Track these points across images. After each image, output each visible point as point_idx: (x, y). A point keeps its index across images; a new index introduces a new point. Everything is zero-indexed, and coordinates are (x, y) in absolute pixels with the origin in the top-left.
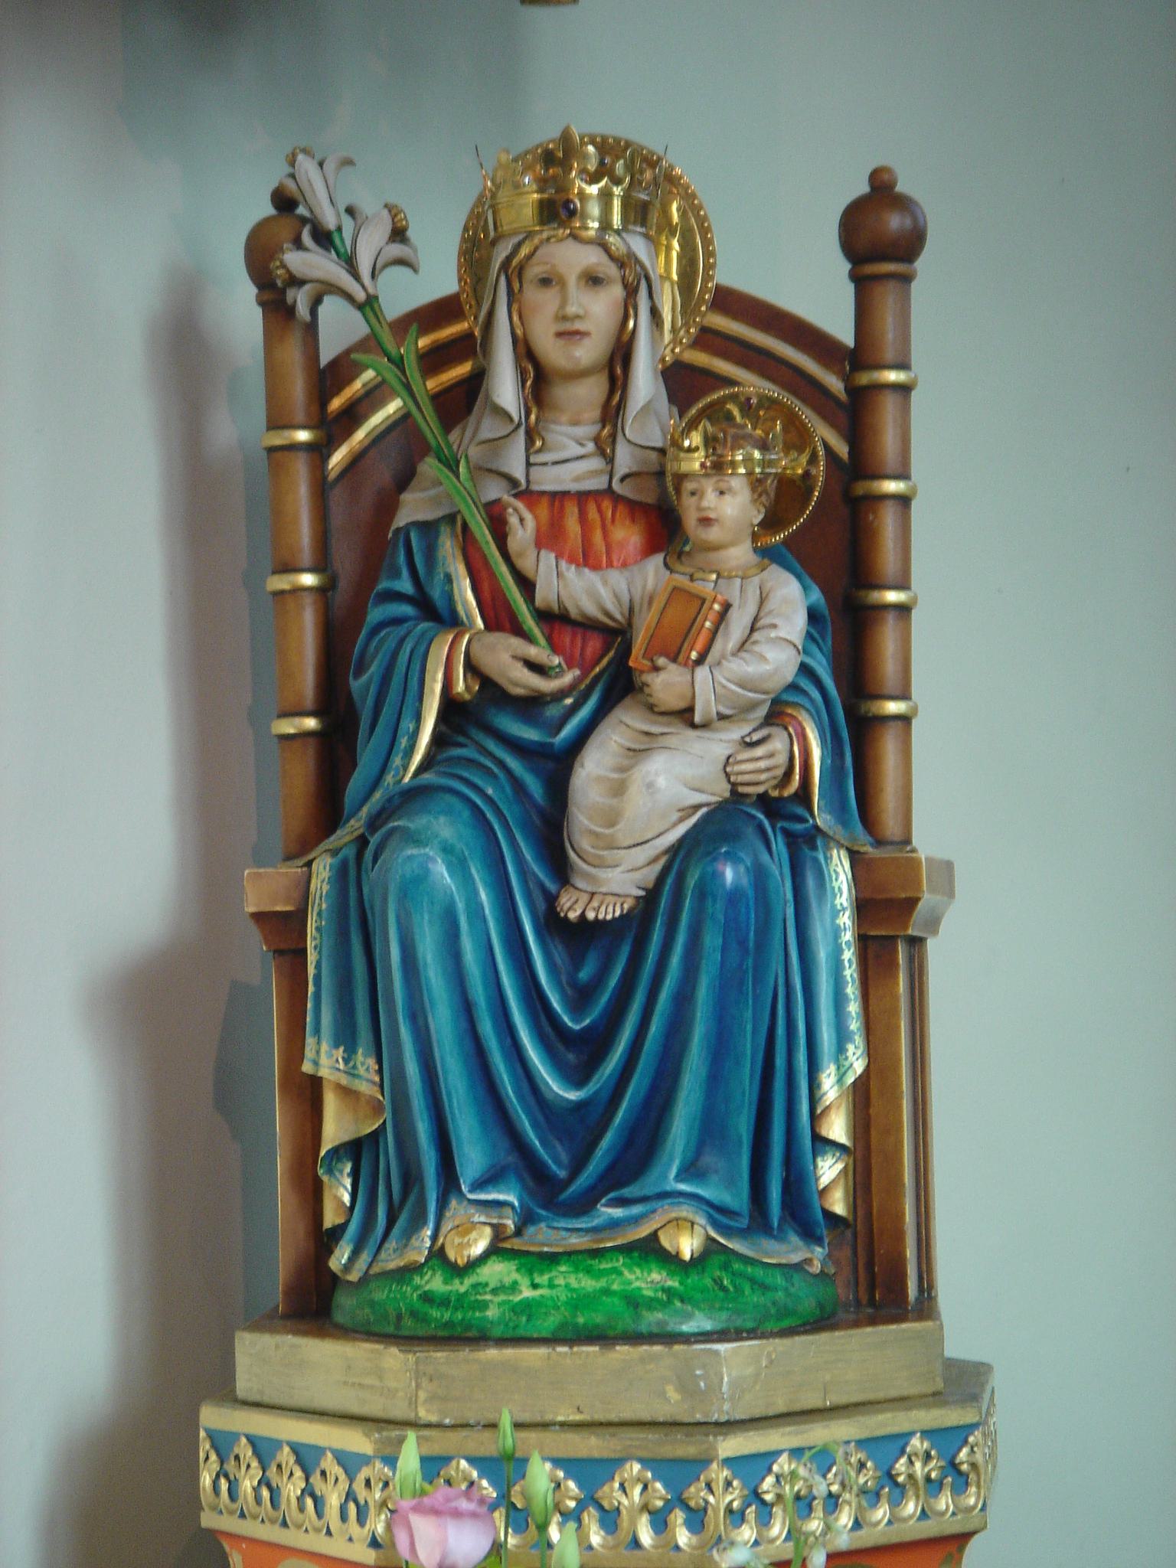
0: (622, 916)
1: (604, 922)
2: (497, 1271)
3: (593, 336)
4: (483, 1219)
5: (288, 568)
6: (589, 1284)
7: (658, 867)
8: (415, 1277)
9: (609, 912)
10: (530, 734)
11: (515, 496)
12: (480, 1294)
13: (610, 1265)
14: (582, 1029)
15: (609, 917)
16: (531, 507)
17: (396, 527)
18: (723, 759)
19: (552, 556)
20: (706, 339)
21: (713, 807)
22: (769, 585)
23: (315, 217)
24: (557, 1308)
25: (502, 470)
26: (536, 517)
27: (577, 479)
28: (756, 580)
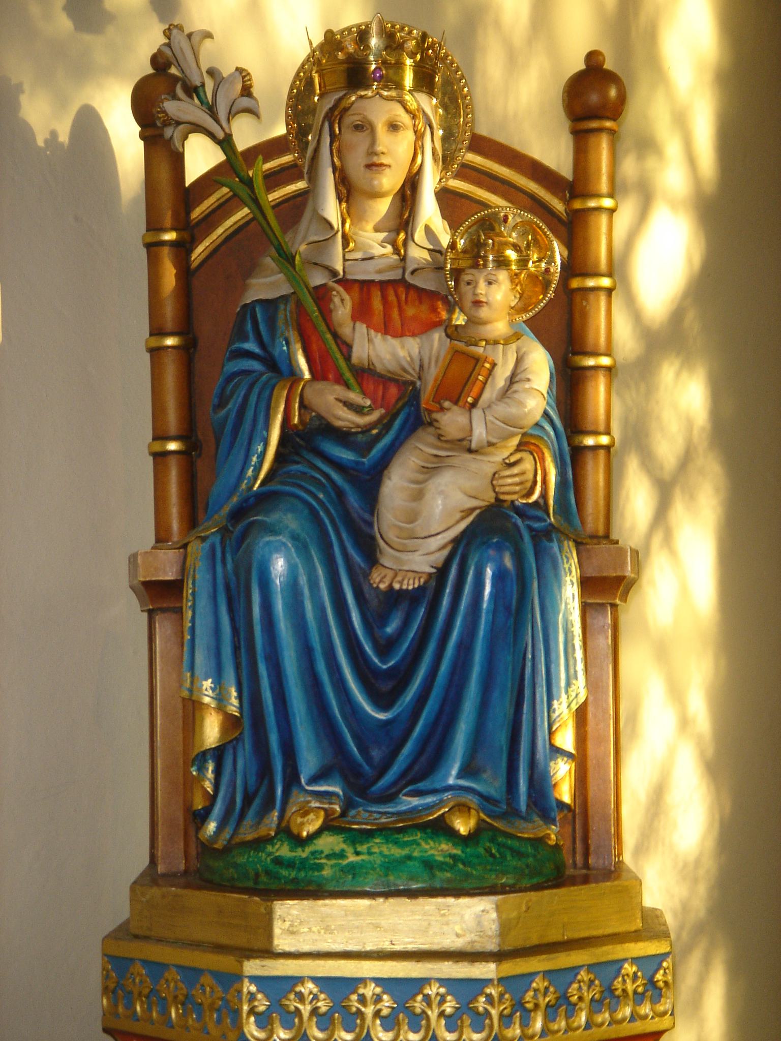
0: (419, 587)
1: (407, 590)
2: (329, 842)
3: (362, 169)
4: (317, 805)
5: (163, 334)
6: (397, 852)
7: (446, 552)
8: (268, 846)
9: (410, 584)
10: (346, 455)
11: (337, 282)
12: (318, 859)
13: (411, 838)
14: (389, 668)
15: (411, 587)
16: (347, 290)
17: (243, 303)
18: (490, 475)
19: (365, 326)
20: (467, 172)
21: (483, 509)
22: (524, 350)
23: (186, 76)
24: (374, 869)
25: (324, 263)
26: (352, 298)
27: (380, 272)
28: (514, 346)
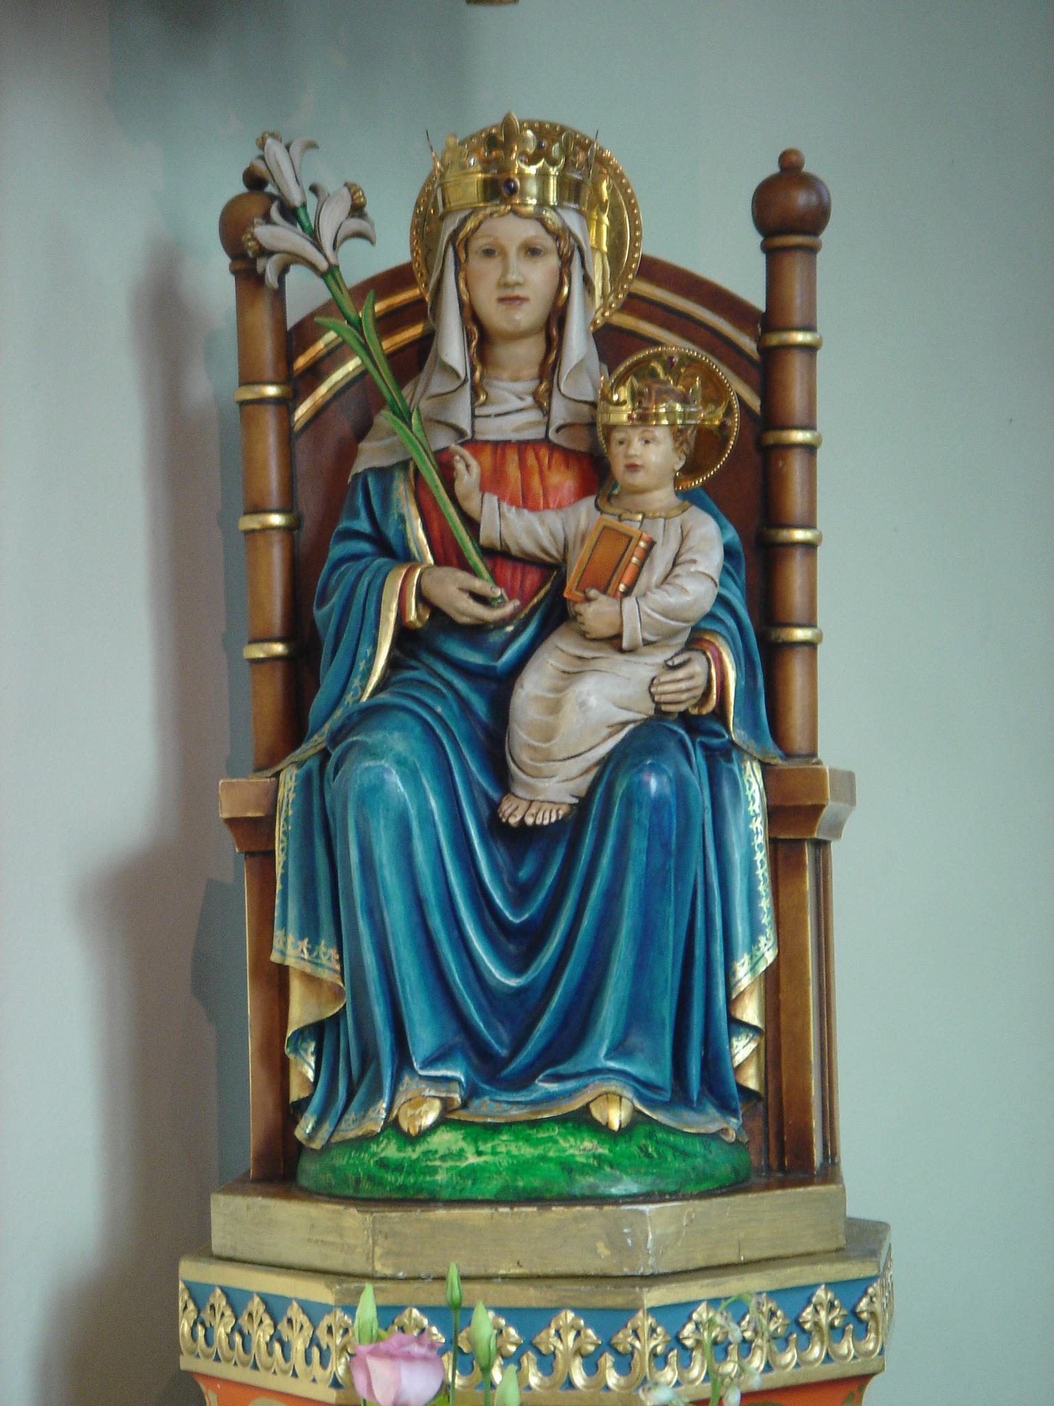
0: (557, 821)
1: (542, 827)
2: (445, 1140)
3: (531, 301)
4: (433, 1093)
5: (258, 509)
6: (528, 1151)
7: (590, 777)
8: (372, 1145)
9: (546, 818)
10: (475, 658)
11: (462, 445)
12: (430, 1160)
13: (546, 1135)
14: (522, 923)
15: (546, 822)
16: (476, 454)
17: (355, 472)
18: (648, 680)
19: (495, 498)
20: (633, 304)
21: (639, 723)
22: (689, 524)
23: (282, 195)
24: (500, 1173)
25: (450, 421)
26: (480, 464)
27: (517, 430)
28: (678, 520)
